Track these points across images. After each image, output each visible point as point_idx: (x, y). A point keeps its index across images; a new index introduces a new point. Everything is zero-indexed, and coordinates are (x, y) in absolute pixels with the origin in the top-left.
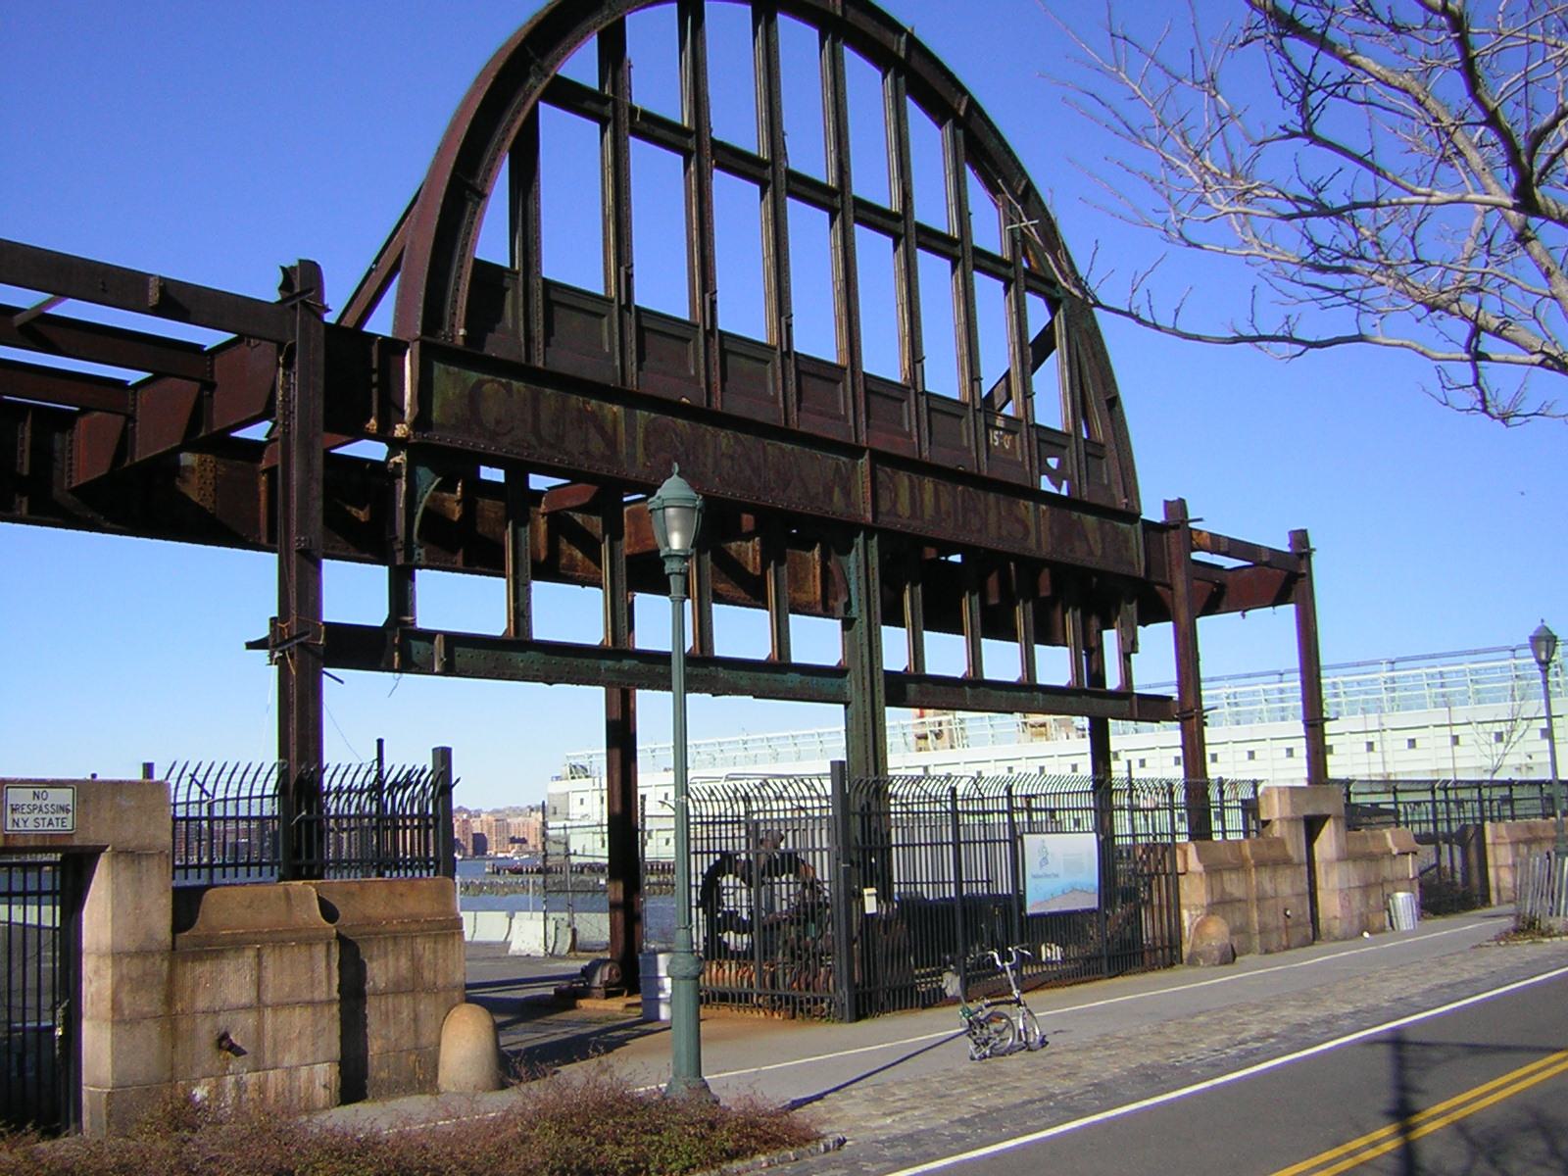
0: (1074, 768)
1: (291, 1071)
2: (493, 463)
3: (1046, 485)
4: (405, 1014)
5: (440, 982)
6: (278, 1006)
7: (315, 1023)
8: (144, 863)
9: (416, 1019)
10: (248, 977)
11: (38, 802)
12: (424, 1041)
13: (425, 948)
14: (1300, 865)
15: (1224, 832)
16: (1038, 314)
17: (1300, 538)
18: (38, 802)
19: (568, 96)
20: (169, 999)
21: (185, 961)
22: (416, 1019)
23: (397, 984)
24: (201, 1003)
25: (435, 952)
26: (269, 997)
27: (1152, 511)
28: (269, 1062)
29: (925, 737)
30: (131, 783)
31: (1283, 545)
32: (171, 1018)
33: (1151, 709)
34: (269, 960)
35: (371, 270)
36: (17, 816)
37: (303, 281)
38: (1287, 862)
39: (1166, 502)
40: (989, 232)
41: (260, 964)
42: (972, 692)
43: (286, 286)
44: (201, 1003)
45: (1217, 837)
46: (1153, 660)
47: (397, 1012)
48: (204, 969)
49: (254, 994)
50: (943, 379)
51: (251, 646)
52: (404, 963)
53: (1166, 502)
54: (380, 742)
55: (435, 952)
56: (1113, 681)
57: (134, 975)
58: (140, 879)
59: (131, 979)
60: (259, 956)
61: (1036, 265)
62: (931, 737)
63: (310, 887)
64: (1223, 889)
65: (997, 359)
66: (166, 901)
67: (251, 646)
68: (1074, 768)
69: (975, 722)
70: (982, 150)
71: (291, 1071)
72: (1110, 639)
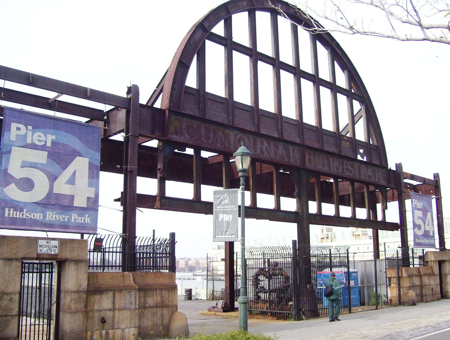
0: (368, 248)
1: (123, 330)
2: (190, 147)
3: (359, 157)
4: (159, 314)
5: (170, 304)
6: (120, 310)
7: (131, 315)
8: (79, 264)
9: (162, 315)
10: (110, 300)
11: (48, 244)
12: (165, 322)
13: (165, 293)
14: (437, 275)
15: (414, 265)
16: (357, 105)
17: (436, 176)
18: (48, 244)
19: (216, 39)
20: (86, 306)
21: (91, 295)
22: (162, 315)
23: (157, 304)
24: (96, 307)
25: (169, 295)
26: (117, 307)
27: (392, 166)
28: (116, 327)
29: (323, 238)
30: (76, 240)
31: (432, 178)
32: (87, 312)
33: (392, 227)
34: (117, 295)
35: (155, 90)
36: (41, 248)
37: (133, 91)
38: (433, 274)
39: (396, 164)
40: (342, 80)
41: (114, 296)
42: (336, 221)
43: (129, 92)
44: (96, 307)
45: (411, 266)
46: (392, 213)
47: (156, 313)
48: (97, 297)
49: (112, 305)
50: (328, 125)
51: (116, 200)
52: (159, 298)
53: (396, 164)
54: (154, 231)
55: (169, 295)
56: (380, 218)
57: (75, 298)
58: (78, 270)
59: (74, 300)
60: (114, 294)
61: (357, 90)
62: (325, 239)
63: (131, 274)
64: (413, 282)
65: (344, 120)
66: (86, 276)
67: (116, 200)
68: (368, 248)
69: (336, 229)
70: (339, 56)
71: (123, 330)
72: (379, 206)
